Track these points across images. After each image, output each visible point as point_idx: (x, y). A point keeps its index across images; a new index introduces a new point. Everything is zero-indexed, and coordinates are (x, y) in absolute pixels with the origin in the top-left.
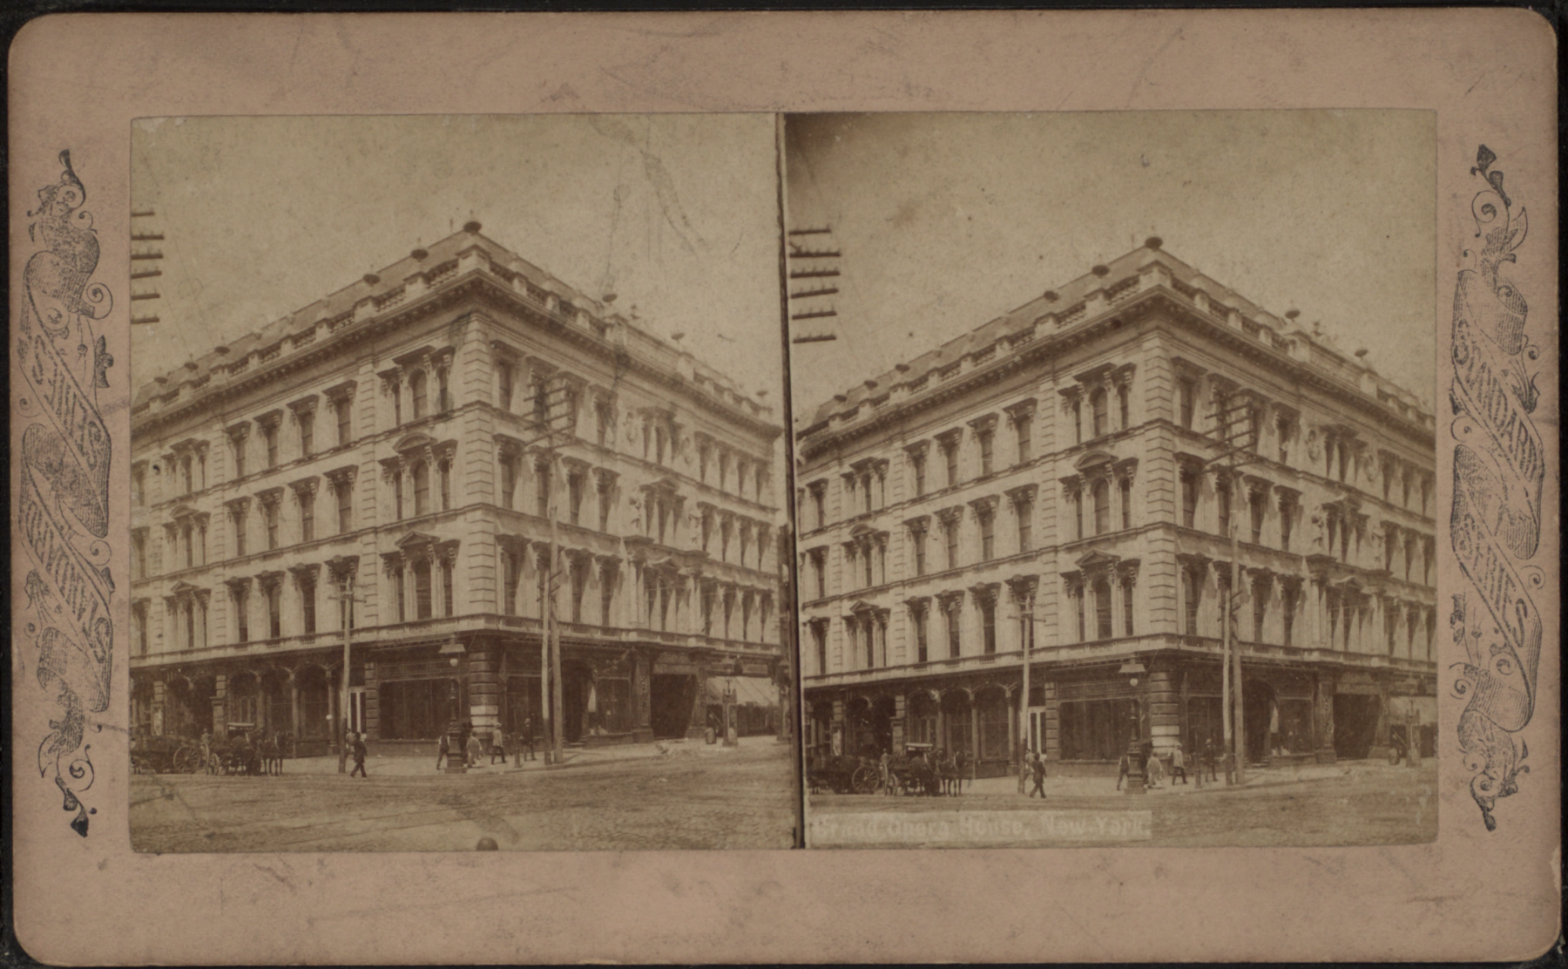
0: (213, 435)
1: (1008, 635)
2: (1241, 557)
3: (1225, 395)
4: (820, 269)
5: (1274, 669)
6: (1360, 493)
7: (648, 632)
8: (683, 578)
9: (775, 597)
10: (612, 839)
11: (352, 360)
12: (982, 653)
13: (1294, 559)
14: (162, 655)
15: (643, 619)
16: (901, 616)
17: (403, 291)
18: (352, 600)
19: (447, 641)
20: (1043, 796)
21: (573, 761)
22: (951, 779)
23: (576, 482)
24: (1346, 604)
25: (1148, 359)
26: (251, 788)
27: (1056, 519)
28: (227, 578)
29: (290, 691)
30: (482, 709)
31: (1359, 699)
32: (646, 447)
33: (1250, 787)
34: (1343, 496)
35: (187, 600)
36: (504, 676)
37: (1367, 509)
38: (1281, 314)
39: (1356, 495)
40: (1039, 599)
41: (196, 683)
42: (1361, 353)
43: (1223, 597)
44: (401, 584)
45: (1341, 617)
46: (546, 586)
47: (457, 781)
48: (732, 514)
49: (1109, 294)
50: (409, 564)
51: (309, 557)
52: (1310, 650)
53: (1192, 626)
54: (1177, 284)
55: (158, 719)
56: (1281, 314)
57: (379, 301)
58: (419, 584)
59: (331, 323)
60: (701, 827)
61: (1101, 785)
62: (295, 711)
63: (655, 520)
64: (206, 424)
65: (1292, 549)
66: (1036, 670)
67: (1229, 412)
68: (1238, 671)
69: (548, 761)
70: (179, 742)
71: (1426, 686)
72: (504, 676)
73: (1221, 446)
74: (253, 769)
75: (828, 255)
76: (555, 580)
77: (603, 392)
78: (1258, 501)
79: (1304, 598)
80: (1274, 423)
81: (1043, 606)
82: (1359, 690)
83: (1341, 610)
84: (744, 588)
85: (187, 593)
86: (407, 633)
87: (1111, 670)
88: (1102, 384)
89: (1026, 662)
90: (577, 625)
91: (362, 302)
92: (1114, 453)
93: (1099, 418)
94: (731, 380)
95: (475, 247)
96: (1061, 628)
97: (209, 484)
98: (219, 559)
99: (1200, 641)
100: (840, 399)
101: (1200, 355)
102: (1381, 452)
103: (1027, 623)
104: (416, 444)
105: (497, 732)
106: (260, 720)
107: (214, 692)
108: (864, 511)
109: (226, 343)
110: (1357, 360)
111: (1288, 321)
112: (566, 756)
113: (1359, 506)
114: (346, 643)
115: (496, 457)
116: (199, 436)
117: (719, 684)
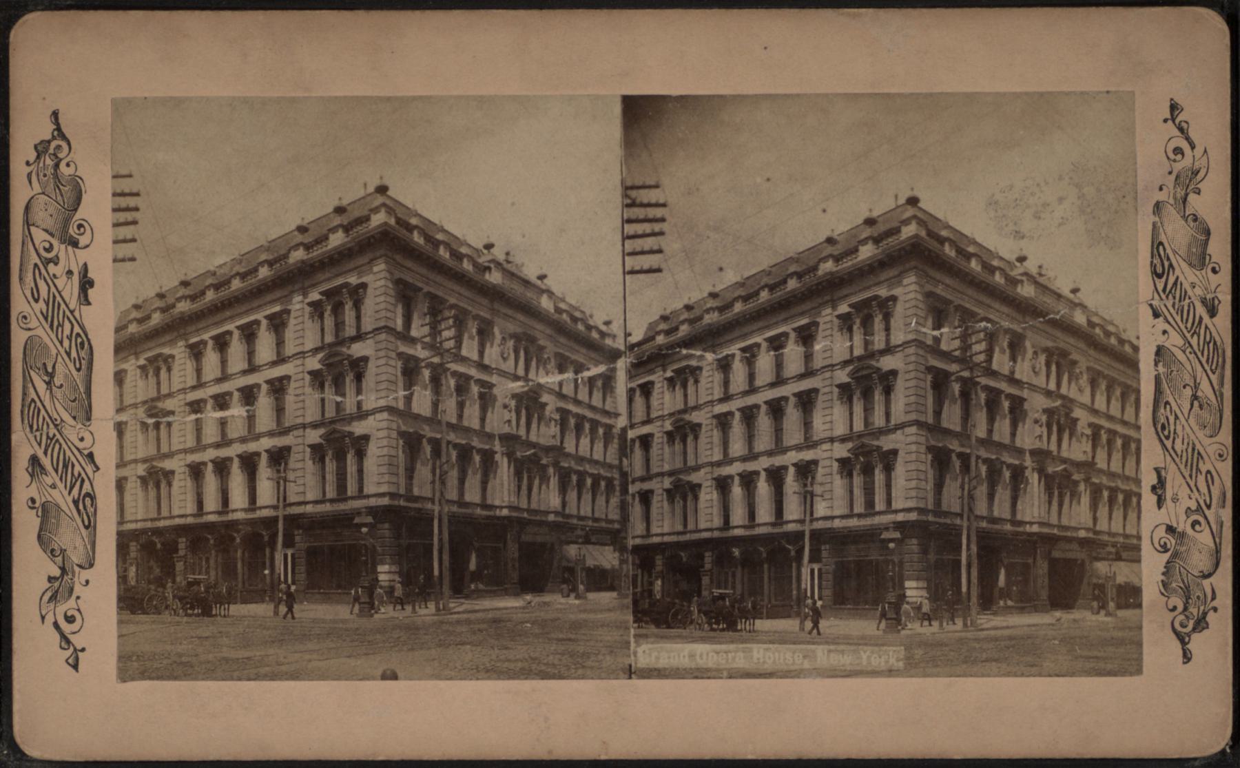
0: (179, 351)
1: (793, 510)
3: (436, 309)
5: (470, 521)
6: (1072, 401)
7: (517, 509)
9: (616, 483)
10: (487, 671)
11: (286, 293)
12: (246, 506)
13: (1020, 452)
14: (136, 521)
15: (513, 499)
16: (182, 476)
17: (327, 239)
18: (285, 480)
19: (359, 514)
21: (985, 626)
23: (461, 390)
24: (1059, 488)
25: (908, 291)
26: (206, 627)
27: (305, 403)
28: (188, 462)
30: (386, 568)
31: (1069, 563)
32: (1048, 376)
33: (982, 630)
34: (1058, 403)
35: (156, 479)
36: (932, 557)
37: (1078, 413)
38: (480, 246)
39: (1068, 402)
40: (292, 465)
41: (163, 544)
42: (1075, 291)
44: (323, 469)
46: (966, 487)
47: (365, 623)
48: (584, 417)
49: (877, 240)
51: (252, 447)
52: (1031, 523)
53: (938, 502)
54: (930, 234)
55: (132, 571)
56: (480, 246)
57: (308, 247)
58: (865, 483)
59: (270, 263)
60: (556, 662)
61: (867, 626)
62: (239, 565)
63: (1054, 437)
64: (172, 343)
65: (1018, 443)
66: (815, 535)
67: (439, 322)
68: (974, 538)
69: (438, 609)
71: (1129, 551)
72: (932, 557)
73: (964, 361)
74: (207, 613)
76: (974, 483)
77: (483, 320)
79: (1027, 483)
81: (821, 484)
82: (1070, 555)
83: (1056, 493)
85: (156, 473)
86: (327, 507)
87: (870, 536)
88: (869, 313)
89: (807, 528)
90: (462, 504)
91: (825, 259)
92: (878, 365)
93: (339, 326)
94: (583, 312)
96: (833, 503)
99: (947, 514)
100: (137, 307)
101: (415, 275)
102: (557, 355)
103: (808, 498)
104: (865, 372)
105: (398, 586)
106: (213, 573)
107: (177, 550)
108: (155, 395)
109: (189, 278)
110: (1071, 296)
111: (1018, 264)
112: (452, 605)
113: (1072, 411)
114: (280, 513)
115: (399, 370)
116: (166, 351)
117: (1102, 567)
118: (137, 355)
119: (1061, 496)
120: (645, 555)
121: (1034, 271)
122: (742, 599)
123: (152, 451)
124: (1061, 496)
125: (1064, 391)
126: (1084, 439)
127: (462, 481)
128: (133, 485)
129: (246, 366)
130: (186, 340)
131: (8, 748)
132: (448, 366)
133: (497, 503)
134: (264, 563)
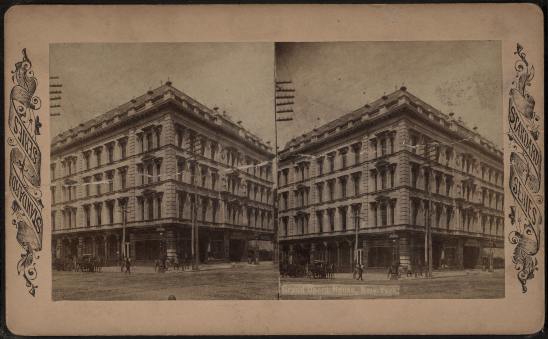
0: (79, 155)
1: (350, 225)
2: (198, 191)
3: (193, 136)
4: (288, 95)
5: (208, 230)
7: (228, 225)
8: (241, 206)
10: (215, 296)
13: (451, 199)
14: (60, 230)
15: (227, 220)
17: (145, 105)
18: (126, 212)
19: (159, 227)
20: (362, 280)
21: (435, 276)
22: (98, 267)
23: (204, 172)
24: (468, 215)
25: (401, 128)
26: (91, 277)
27: (135, 178)
28: (83, 204)
29: (104, 243)
30: (171, 251)
31: (473, 248)
32: (463, 166)
33: (434, 278)
35: (69, 211)
36: (412, 246)
38: (212, 109)
39: (472, 177)
40: (129, 205)
41: (72, 240)
42: (475, 128)
43: (426, 212)
44: (143, 207)
45: (232, 213)
46: (427, 215)
47: (162, 275)
48: (258, 184)
49: (387, 106)
50: (146, 200)
51: (111, 197)
52: (456, 231)
53: (414, 222)
54: (411, 103)
55: (58, 252)
56: (212, 109)
57: (136, 109)
58: (382, 213)
59: (120, 116)
61: (383, 276)
63: (466, 193)
64: (76, 151)
65: (450, 196)
66: (360, 236)
67: (194, 142)
68: (430, 238)
69: (194, 269)
70: (66, 260)
71: (499, 243)
72: (412, 246)
73: (426, 159)
74: (91, 270)
75: (290, 91)
76: (430, 213)
78: (438, 180)
80: (444, 152)
81: (363, 214)
82: (473, 245)
84: (261, 210)
85: (69, 209)
87: (385, 236)
88: (384, 138)
89: (357, 233)
90: (204, 222)
91: (364, 114)
92: (154, 155)
94: (258, 138)
95: (404, 96)
96: (368, 222)
97: (78, 170)
98: (80, 197)
101: (183, 121)
102: (246, 157)
103: (357, 220)
104: (382, 164)
106: (94, 253)
107: (78, 243)
108: (69, 174)
110: (473, 131)
111: (450, 117)
112: (200, 267)
113: (474, 181)
115: (176, 163)
116: (73, 155)
117: (487, 250)
118: (60, 157)
119: (469, 219)
120: (285, 245)
121: (457, 119)
122: (328, 265)
123: (67, 199)
124: (469, 219)
125: (470, 172)
126: (479, 194)
127: (204, 212)
128: (59, 214)
129: (109, 162)
130: (82, 150)
131: (4, 330)
132: (198, 161)
133: (220, 222)
134: (117, 249)
